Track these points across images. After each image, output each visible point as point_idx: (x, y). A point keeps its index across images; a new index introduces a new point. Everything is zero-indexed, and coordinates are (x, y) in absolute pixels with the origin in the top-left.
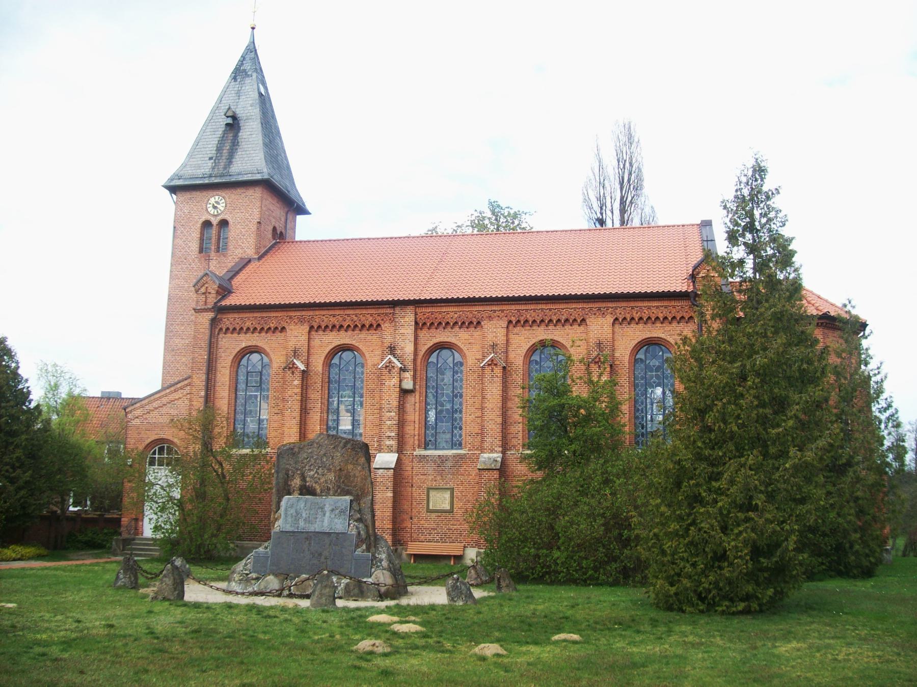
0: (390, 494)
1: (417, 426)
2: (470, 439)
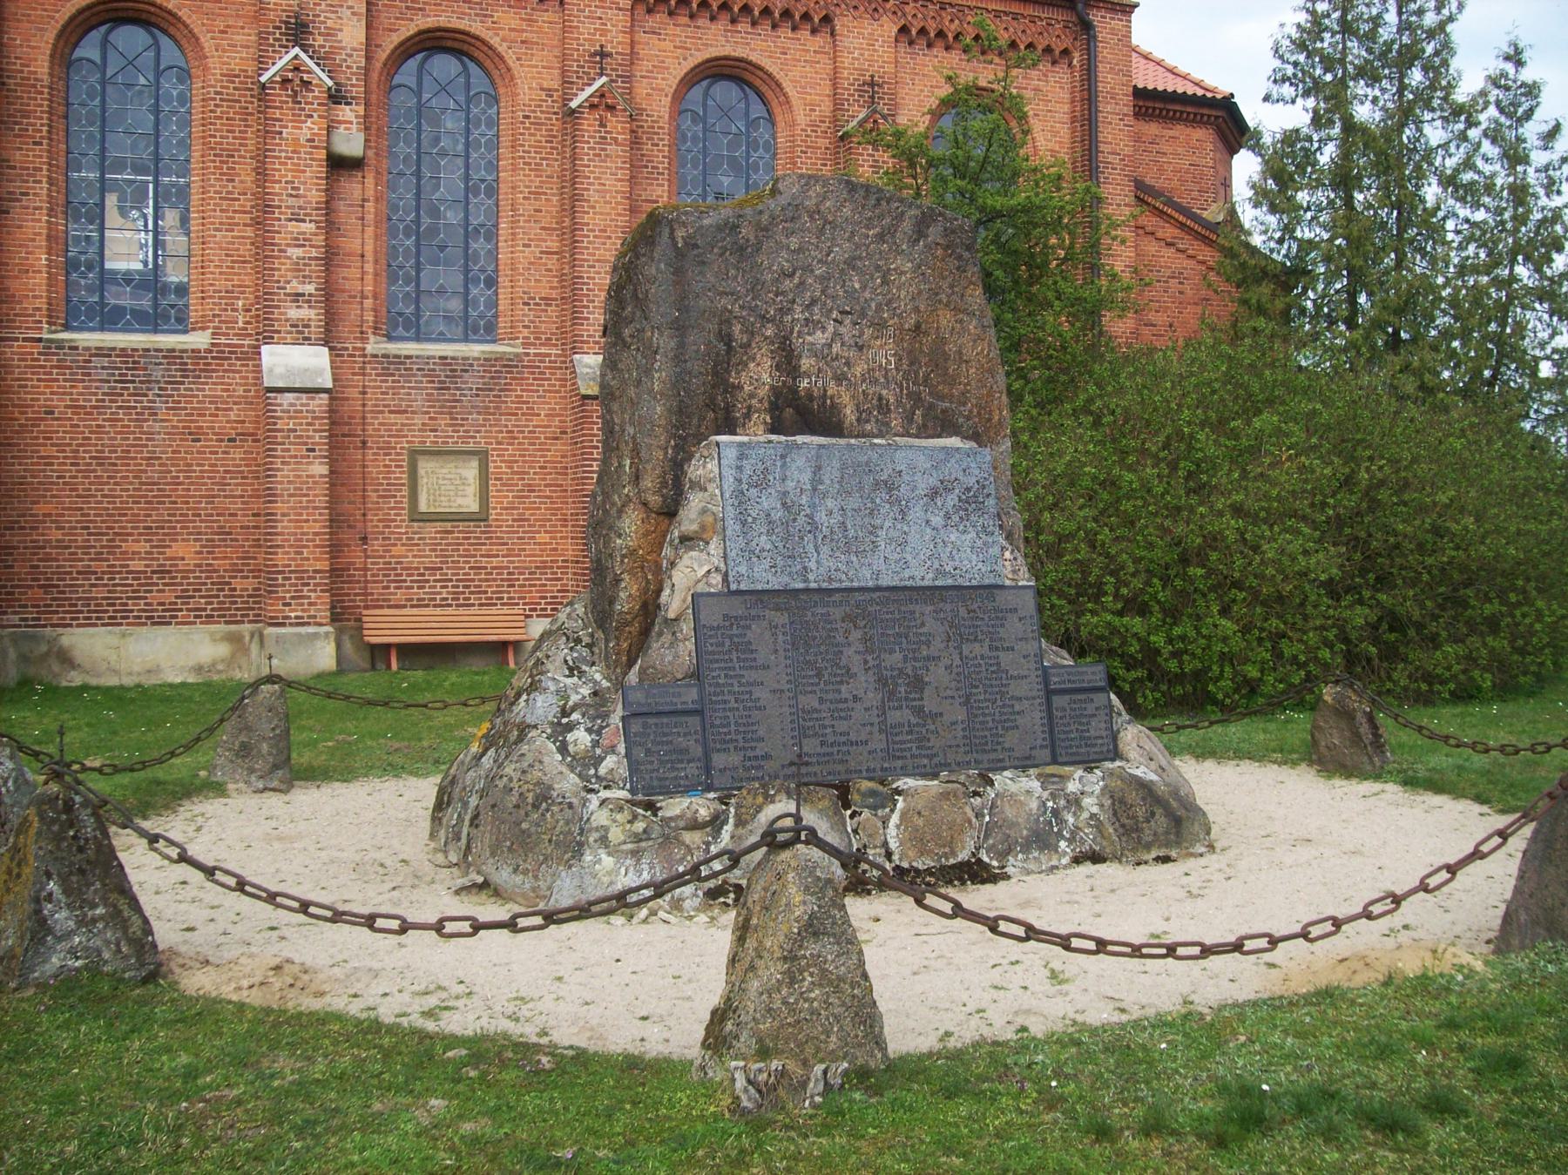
0: (320, 469)
1: (369, 268)
2: (525, 314)
